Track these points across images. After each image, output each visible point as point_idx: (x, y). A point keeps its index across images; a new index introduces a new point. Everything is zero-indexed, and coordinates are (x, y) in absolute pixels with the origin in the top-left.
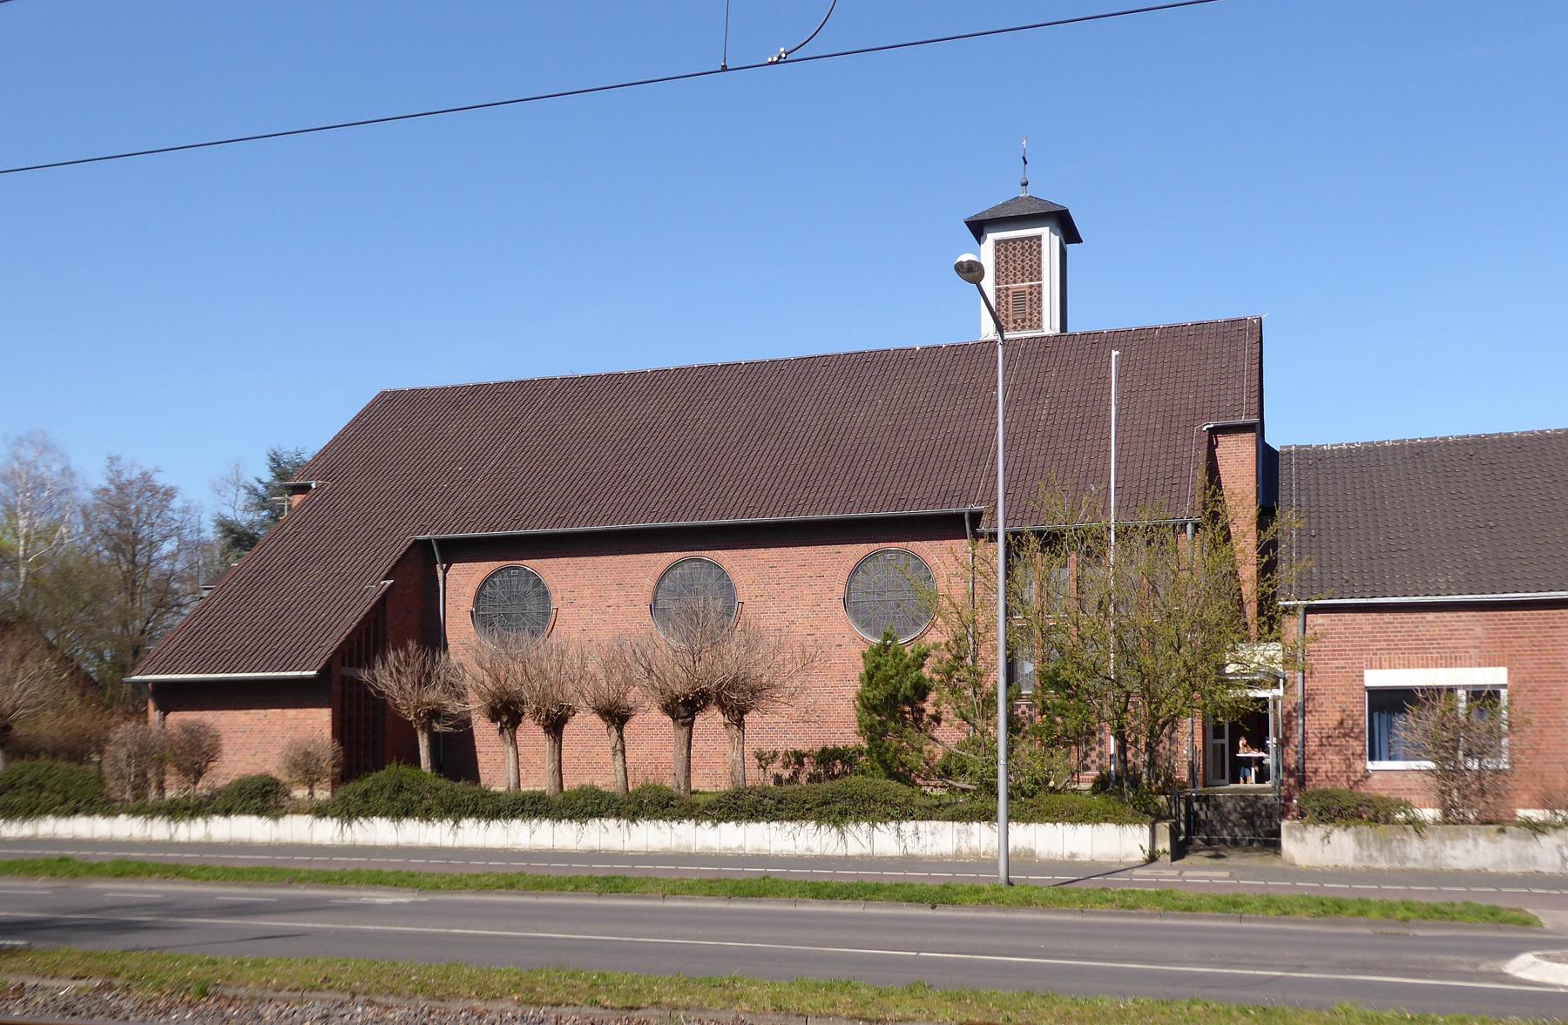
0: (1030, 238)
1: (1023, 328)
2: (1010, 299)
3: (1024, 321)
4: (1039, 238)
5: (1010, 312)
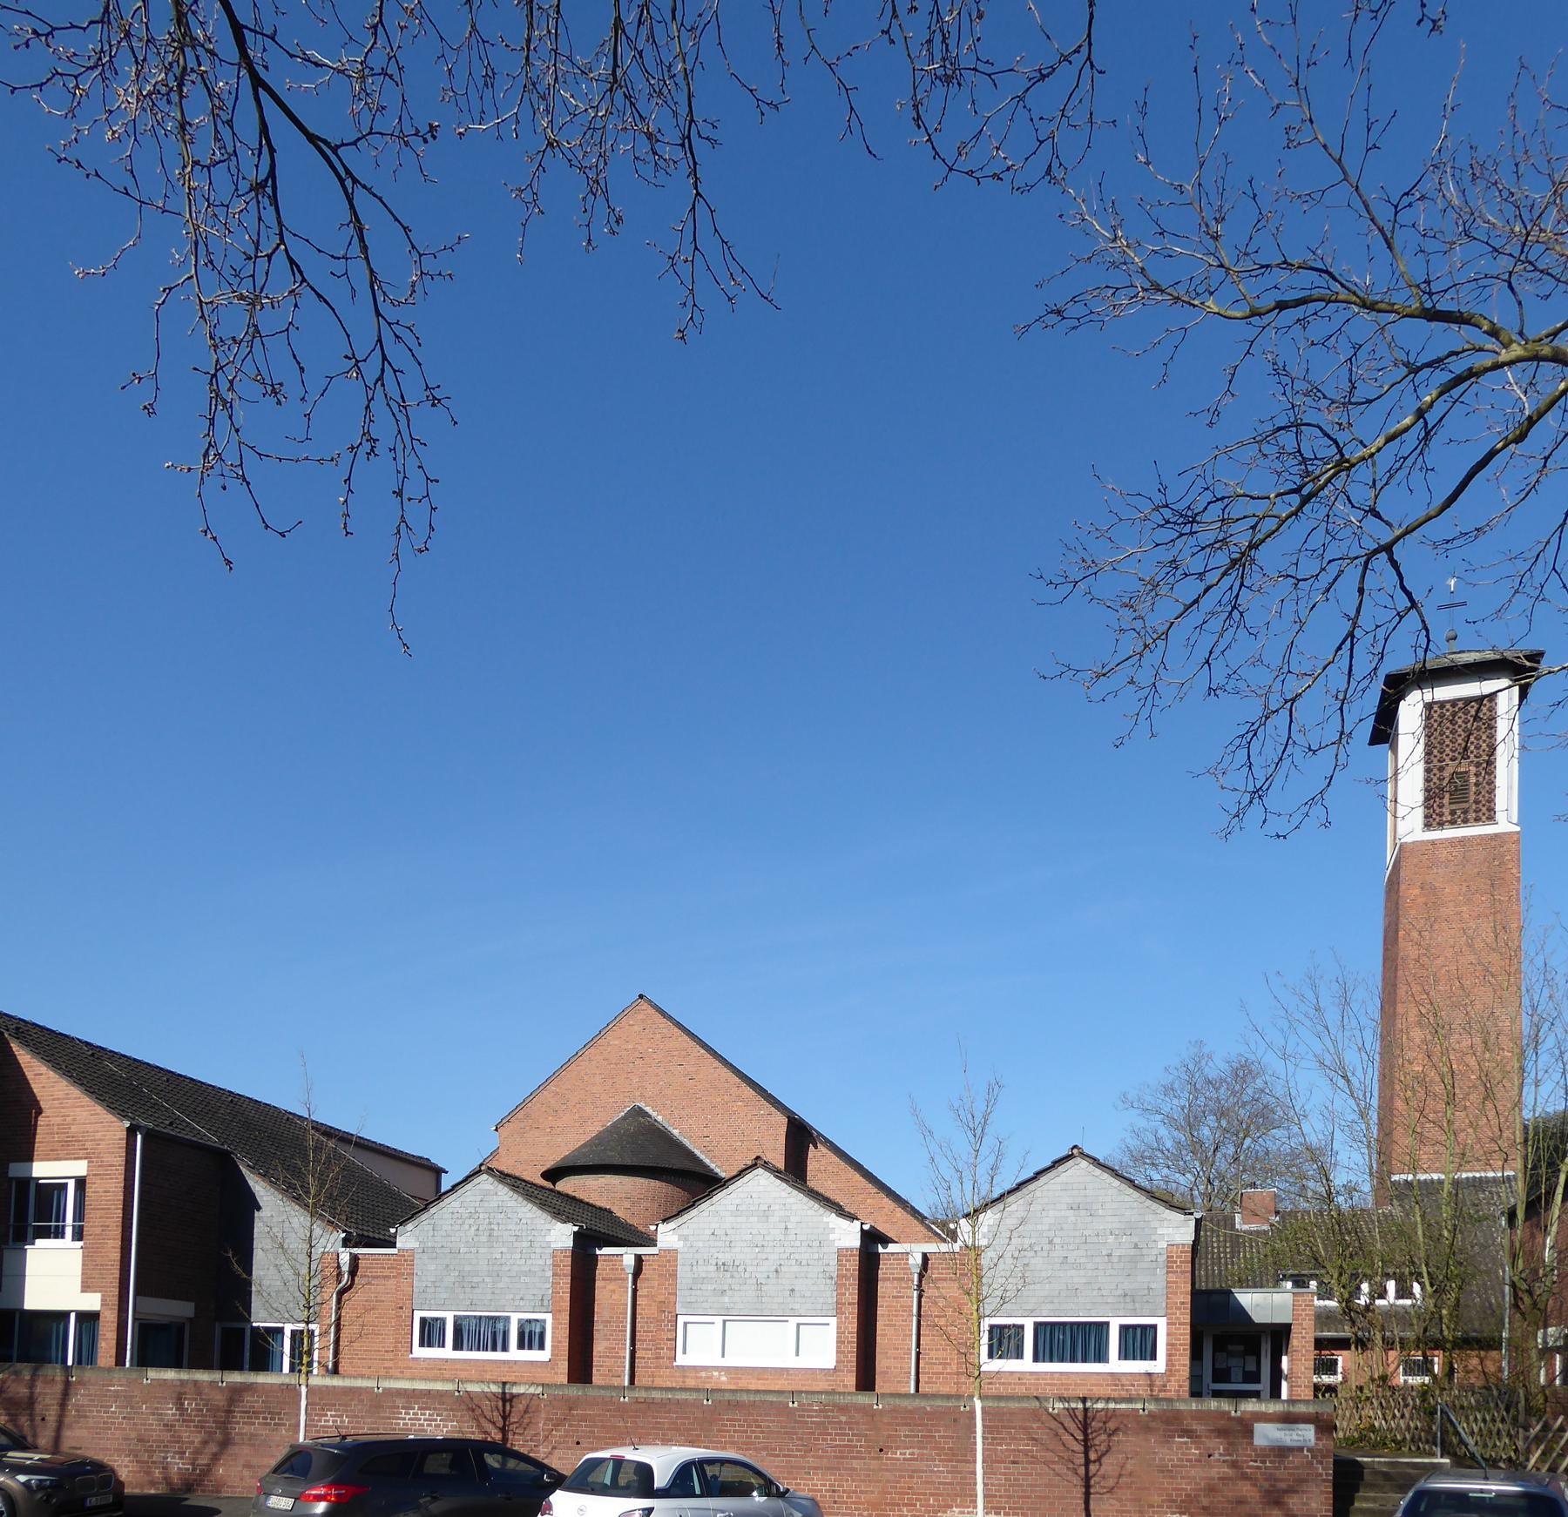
1: (1465, 821)
3: (1465, 812)
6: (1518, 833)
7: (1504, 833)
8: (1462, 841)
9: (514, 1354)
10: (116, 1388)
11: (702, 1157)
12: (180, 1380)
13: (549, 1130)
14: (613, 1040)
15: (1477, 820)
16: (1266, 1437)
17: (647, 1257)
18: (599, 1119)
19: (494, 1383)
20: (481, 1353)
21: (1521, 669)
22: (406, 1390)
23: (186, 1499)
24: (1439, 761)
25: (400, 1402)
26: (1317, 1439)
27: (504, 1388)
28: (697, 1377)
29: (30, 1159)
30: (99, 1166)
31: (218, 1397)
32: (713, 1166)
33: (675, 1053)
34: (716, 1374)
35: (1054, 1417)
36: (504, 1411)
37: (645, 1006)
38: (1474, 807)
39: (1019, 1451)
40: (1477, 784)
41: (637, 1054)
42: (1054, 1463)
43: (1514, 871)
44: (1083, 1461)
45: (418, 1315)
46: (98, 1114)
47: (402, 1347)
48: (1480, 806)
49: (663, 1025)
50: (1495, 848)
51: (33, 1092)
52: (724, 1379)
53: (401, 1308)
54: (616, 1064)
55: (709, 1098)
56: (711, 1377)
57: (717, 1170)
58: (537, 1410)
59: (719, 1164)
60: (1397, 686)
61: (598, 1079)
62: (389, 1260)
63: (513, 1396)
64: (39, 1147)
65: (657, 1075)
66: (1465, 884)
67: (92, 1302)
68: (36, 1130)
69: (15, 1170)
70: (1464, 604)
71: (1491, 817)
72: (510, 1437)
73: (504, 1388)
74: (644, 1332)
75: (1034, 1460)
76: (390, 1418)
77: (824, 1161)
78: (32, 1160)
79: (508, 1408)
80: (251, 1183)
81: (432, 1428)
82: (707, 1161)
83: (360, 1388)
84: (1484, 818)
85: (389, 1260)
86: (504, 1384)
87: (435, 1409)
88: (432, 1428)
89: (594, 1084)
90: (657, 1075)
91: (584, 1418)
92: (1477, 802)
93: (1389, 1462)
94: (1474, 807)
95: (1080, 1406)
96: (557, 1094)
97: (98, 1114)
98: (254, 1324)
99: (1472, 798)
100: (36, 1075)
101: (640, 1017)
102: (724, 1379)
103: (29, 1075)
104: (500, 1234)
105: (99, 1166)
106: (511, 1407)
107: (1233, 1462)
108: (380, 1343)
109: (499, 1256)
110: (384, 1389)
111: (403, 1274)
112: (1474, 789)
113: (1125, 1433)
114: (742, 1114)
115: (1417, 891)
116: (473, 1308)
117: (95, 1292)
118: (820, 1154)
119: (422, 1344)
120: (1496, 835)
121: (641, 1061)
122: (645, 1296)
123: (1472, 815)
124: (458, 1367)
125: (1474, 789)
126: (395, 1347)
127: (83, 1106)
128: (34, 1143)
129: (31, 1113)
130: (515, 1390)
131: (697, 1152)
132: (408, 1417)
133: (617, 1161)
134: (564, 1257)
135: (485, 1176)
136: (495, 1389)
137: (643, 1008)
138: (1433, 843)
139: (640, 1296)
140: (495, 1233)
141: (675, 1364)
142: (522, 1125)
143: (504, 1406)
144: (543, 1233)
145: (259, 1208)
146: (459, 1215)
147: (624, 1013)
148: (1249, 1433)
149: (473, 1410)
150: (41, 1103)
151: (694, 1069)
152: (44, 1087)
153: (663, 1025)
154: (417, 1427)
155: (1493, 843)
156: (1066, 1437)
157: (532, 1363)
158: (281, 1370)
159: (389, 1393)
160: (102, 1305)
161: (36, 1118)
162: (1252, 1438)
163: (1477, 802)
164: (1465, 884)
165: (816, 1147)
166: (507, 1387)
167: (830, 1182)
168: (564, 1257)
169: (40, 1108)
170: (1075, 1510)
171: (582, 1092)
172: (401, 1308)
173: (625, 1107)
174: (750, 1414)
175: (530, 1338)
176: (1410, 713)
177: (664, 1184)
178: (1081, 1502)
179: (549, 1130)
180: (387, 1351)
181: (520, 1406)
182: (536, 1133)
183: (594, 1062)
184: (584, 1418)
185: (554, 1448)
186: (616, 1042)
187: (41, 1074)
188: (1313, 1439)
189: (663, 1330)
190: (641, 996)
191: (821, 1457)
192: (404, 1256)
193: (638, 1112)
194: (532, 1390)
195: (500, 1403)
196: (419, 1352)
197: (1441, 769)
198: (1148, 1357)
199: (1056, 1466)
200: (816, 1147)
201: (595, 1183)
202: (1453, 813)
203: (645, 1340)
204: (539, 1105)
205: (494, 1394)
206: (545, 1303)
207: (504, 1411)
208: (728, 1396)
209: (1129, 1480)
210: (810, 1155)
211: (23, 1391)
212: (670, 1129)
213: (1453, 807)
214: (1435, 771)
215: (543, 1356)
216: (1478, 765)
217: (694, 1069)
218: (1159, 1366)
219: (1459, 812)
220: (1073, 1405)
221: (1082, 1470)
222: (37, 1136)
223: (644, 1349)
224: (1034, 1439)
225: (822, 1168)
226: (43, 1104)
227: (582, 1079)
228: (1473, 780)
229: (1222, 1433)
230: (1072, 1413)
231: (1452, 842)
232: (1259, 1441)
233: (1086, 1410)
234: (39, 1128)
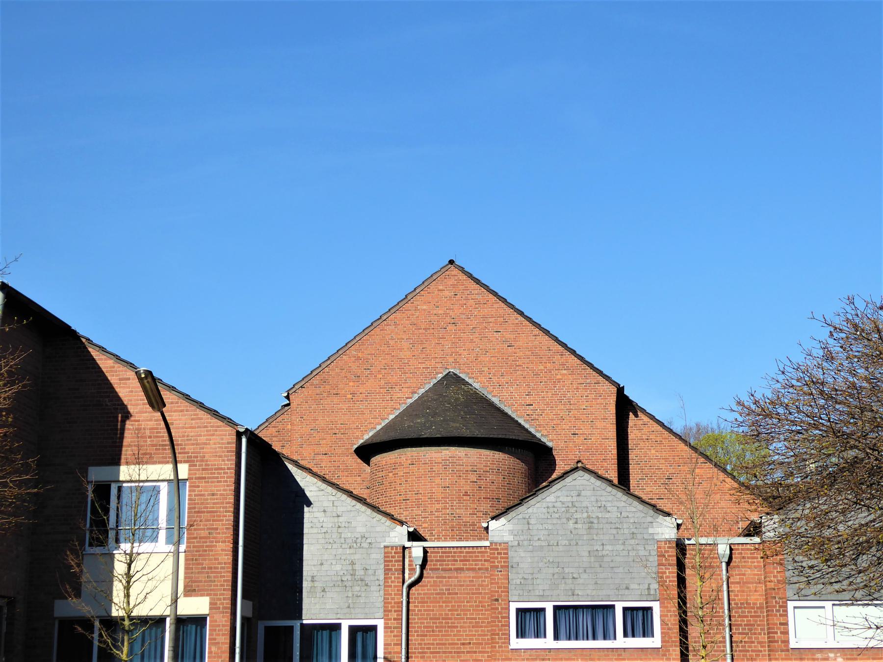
11: (527, 426)
13: (350, 396)
14: (421, 304)
17: (736, 547)
18: (407, 385)
29: (116, 461)
30: (203, 470)
32: (538, 435)
33: (490, 320)
37: (455, 272)
41: (448, 320)
45: (513, 607)
46: (201, 419)
47: (501, 639)
49: (476, 292)
51: (118, 397)
53: (497, 600)
55: (531, 366)
57: (544, 440)
59: (545, 433)
61: (405, 344)
62: (461, 552)
74: (739, 616)
78: (119, 465)
80: (298, 479)
82: (532, 430)
85: (461, 552)
89: (401, 350)
90: (472, 341)
96: (359, 358)
97: (201, 419)
98: (305, 622)
100: (120, 379)
101: (452, 281)
103: (113, 379)
104: (601, 526)
105: (203, 470)
108: (455, 635)
109: (600, 548)
111: (497, 567)
116: (575, 598)
117: (202, 595)
118: (641, 422)
119: (625, 635)
121: (453, 327)
122: (738, 583)
126: (492, 639)
127: (182, 411)
133: (466, 433)
134: (669, 547)
139: (733, 583)
141: (510, 648)
144: (645, 525)
145: (309, 504)
146: (556, 510)
150: (129, 407)
151: (512, 336)
152: (132, 392)
153: (476, 292)
160: (211, 609)
165: (636, 416)
167: (653, 452)
168: (669, 547)
169: (129, 412)
172: (497, 600)
173: (438, 373)
177: (507, 456)
179: (350, 396)
180: (463, 644)
182: (336, 400)
186: (425, 307)
187: (129, 379)
189: (776, 615)
190: (451, 262)
192: (497, 549)
193: (452, 380)
198: (385, 634)
200: (636, 416)
201: (434, 455)
203: (741, 625)
204: (337, 370)
206: (652, 592)
210: (631, 423)
212: (490, 397)
215: (655, 641)
217: (512, 336)
218: (655, 641)
222: (125, 440)
223: (739, 634)
225: (644, 437)
226: (131, 409)
227: (388, 344)
234: (126, 432)
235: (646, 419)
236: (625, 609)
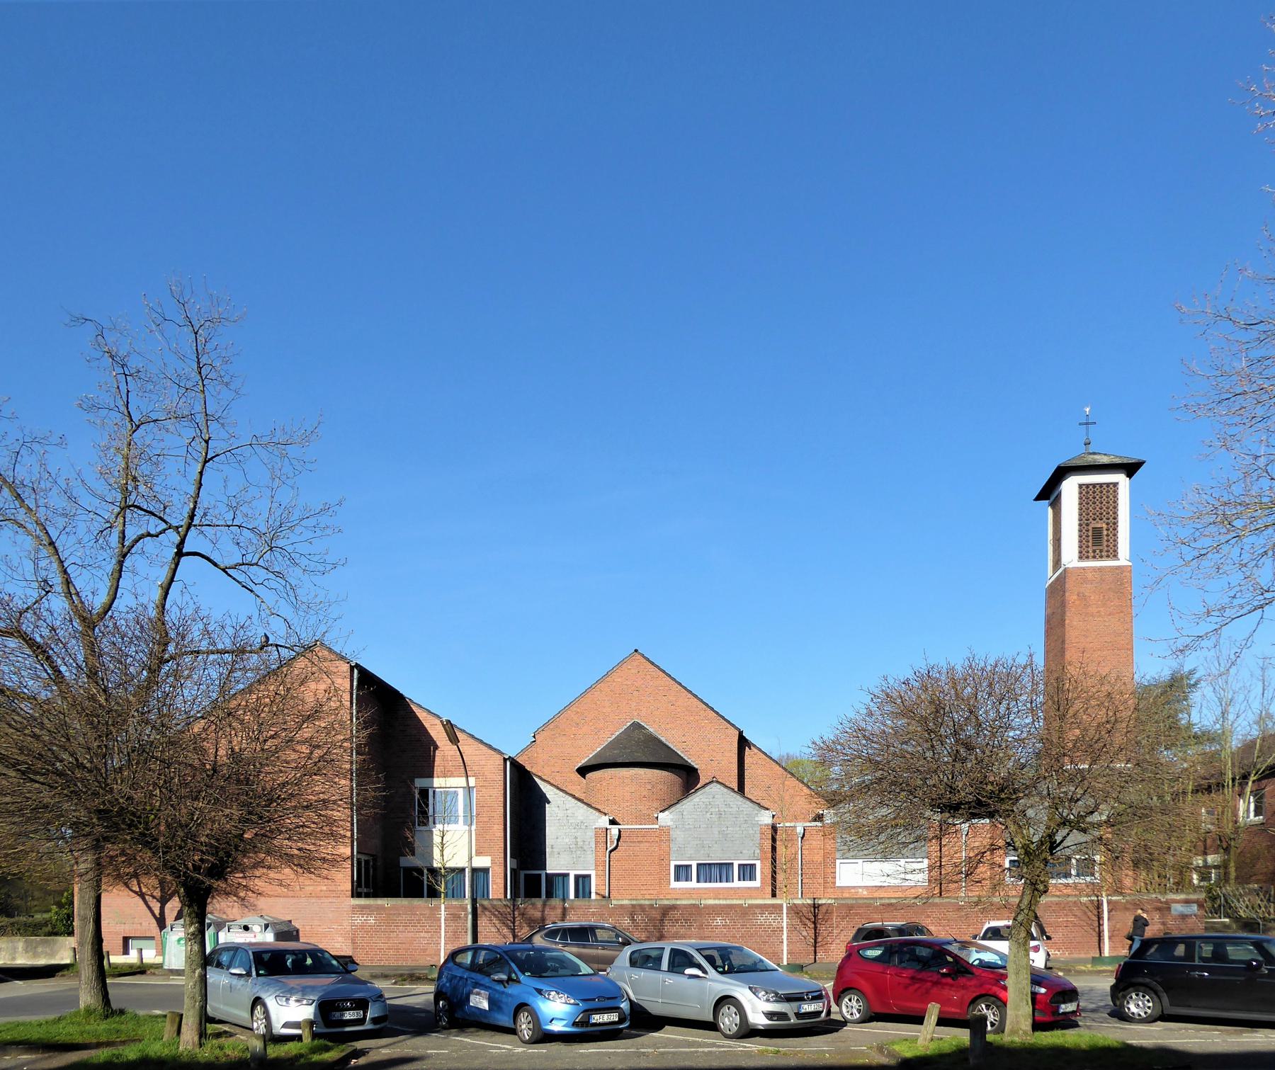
0: (1108, 485)
1: (1101, 557)
2: (1090, 534)
3: (1101, 551)
4: (1115, 484)
5: (1090, 544)
6: (1131, 566)
7: (1124, 566)
8: (1100, 569)
9: (737, 884)
10: (593, 910)
12: (632, 905)
15: (1108, 556)
16: (1176, 910)
19: (809, 898)
20: (728, 883)
21: (1130, 469)
22: (761, 904)
23: (371, 983)
24: (1086, 520)
25: (758, 911)
26: (1198, 910)
27: (814, 901)
28: (849, 893)
29: (431, 776)
31: (654, 913)
32: (689, 761)
34: (860, 890)
35: (1085, 904)
36: (815, 912)
37: (639, 657)
38: (1106, 549)
39: (1068, 921)
40: (1108, 535)
42: (1085, 926)
43: (1129, 589)
44: (1097, 925)
45: (673, 864)
48: (1109, 549)
50: (1118, 574)
52: (865, 893)
54: (620, 694)
56: (858, 892)
58: (832, 913)
60: (1061, 473)
63: (819, 905)
64: (437, 770)
65: (649, 702)
66: (1102, 595)
67: (482, 862)
68: (434, 758)
69: (420, 783)
70: (1095, 423)
71: (1115, 556)
72: (819, 926)
73: (814, 901)
75: (1075, 925)
76: (752, 919)
77: (755, 758)
79: (817, 911)
81: (776, 924)
83: (735, 904)
84: (1111, 556)
86: (814, 899)
87: (777, 914)
88: (776, 924)
90: (649, 702)
91: (856, 914)
92: (1108, 546)
93: (890, 937)
94: (1106, 549)
95: (1096, 898)
99: (1105, 543)
100: (431, 725)
102: (865, 893)
103: (427, 725)
106: (818, 910)
107: (1163, 922)
110: (748, 904)
112: (1106, 538)
113: (1116, 911)
114: (708, 729)
115: (1075, 597)
120: (1119, 567)
123: (1104, 554)
124: (700, 892)
125: (1106, 538)
128: (434, 766)
129: (430, 748)
130: (820, 902)
131: (678, 752)
132: (363, 919)
135: (715, 784)
136: (810, 902)
137: (637, 658)
138: (1084, 569)
140: (723, 816)
142: (553, 733)
143: (815, 910)
147: (623, 662)
148: (1169, 909)
149: (798, 913)
154: (768, 923)
155: (1117, 571)
156: (1090, 914)
157: (749, 888)
158: (465, 897)
159: (751, 906)
161: (434, 751)
162: (1170, 911)
163: (1108, 546)
164: (1102, 595)
165: (750, 749)
166: (816, 900)
170: (1094, 948)
171: (596, 712)
174: (940, 909)
175: (747, 872)
176: (1070, 488)
178: (1097, 944)
181: (823, 909)
182: (564, 738)
183: (604, 693)
184: (856, 914)
185: (842, 930)
188: (1196, 911)
190: (636, 651)
191: (976, 928)
193: (637, 726)
194: (829, 902)
195: (812, 909)
196: (675, 885)
197: (1087, 525)
199: (1085, 928)
200: (750, 749)
201: (627, 773)
202: (1094, 551)
205: (808, 904)
206: (756, 855)
207: (815, 912)
208: (887, 901)
209: (1117, 932)
211: (538, 914)
213: (1095, 548)
214: (1084, 526)
216: (1108, 524)
219: (1098, 551)
220: (1093, 898)
221: (1097, 929)
224: (1074, 915)
228: (1105, 533)
229: (1159, 909)
230: (1092, 901)
231: (1094, 569)
232: (1173, 912)
233: (1098, 900)
235: (756, 751)
236: (740, 865)
